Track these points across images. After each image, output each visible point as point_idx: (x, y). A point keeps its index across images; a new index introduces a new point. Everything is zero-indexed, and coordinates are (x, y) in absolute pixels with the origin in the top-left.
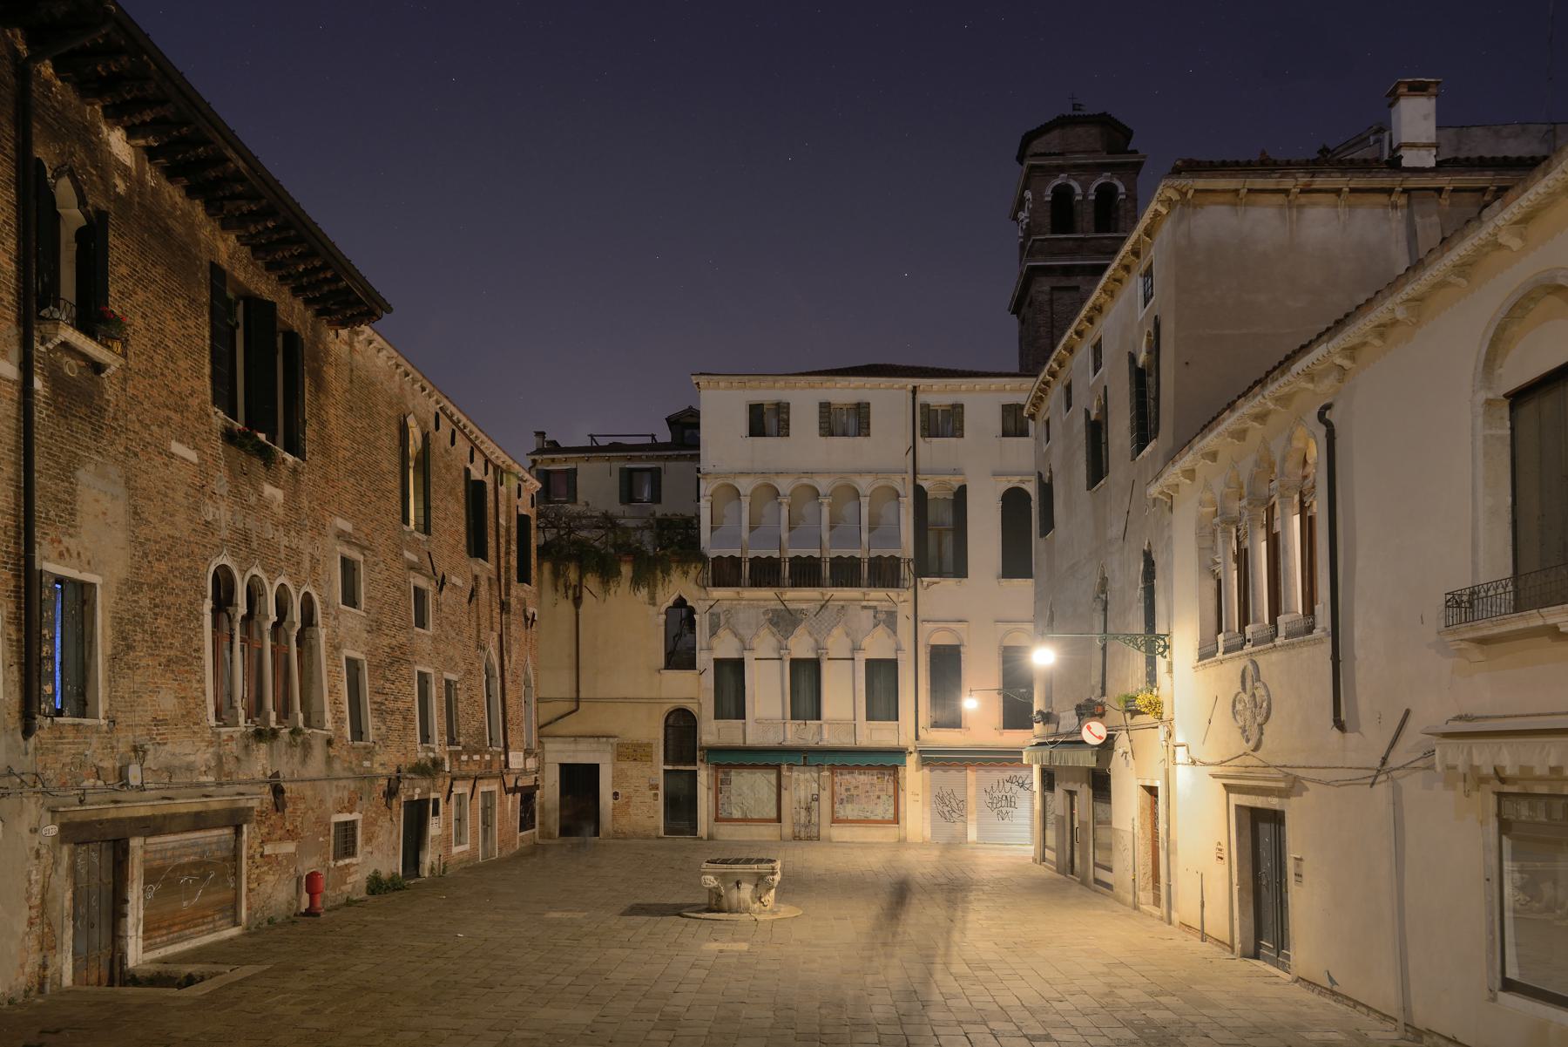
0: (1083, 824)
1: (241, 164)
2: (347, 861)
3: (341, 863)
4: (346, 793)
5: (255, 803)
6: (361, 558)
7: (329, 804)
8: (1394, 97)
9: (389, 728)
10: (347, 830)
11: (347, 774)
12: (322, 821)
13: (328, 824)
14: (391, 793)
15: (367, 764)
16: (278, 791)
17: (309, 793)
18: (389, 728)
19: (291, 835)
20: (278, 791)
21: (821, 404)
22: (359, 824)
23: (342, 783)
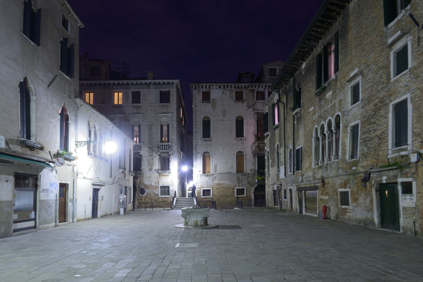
0: (272, 166)
1: (297, 51)
2: (346, 207)
3: (343, 207)
4: (343, 181)
5: (318, 184)
6: (392, 54)
7: (337, 185)
8: (114, 92)
9: (369, 148)
10: (344, 195)
11: (343, 174)
12: (335, 191)
13: (337, 192)
14: (366, 179)
15: (354, 168)
16: (323, 181)
17: (331, 181)
18: (369, 148)
19: (327, 194)
20: (323, 181)
21: (209, 137)
22: (349, 193)
23: (341, 177)
